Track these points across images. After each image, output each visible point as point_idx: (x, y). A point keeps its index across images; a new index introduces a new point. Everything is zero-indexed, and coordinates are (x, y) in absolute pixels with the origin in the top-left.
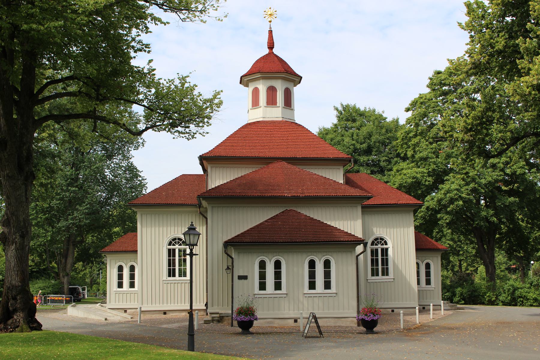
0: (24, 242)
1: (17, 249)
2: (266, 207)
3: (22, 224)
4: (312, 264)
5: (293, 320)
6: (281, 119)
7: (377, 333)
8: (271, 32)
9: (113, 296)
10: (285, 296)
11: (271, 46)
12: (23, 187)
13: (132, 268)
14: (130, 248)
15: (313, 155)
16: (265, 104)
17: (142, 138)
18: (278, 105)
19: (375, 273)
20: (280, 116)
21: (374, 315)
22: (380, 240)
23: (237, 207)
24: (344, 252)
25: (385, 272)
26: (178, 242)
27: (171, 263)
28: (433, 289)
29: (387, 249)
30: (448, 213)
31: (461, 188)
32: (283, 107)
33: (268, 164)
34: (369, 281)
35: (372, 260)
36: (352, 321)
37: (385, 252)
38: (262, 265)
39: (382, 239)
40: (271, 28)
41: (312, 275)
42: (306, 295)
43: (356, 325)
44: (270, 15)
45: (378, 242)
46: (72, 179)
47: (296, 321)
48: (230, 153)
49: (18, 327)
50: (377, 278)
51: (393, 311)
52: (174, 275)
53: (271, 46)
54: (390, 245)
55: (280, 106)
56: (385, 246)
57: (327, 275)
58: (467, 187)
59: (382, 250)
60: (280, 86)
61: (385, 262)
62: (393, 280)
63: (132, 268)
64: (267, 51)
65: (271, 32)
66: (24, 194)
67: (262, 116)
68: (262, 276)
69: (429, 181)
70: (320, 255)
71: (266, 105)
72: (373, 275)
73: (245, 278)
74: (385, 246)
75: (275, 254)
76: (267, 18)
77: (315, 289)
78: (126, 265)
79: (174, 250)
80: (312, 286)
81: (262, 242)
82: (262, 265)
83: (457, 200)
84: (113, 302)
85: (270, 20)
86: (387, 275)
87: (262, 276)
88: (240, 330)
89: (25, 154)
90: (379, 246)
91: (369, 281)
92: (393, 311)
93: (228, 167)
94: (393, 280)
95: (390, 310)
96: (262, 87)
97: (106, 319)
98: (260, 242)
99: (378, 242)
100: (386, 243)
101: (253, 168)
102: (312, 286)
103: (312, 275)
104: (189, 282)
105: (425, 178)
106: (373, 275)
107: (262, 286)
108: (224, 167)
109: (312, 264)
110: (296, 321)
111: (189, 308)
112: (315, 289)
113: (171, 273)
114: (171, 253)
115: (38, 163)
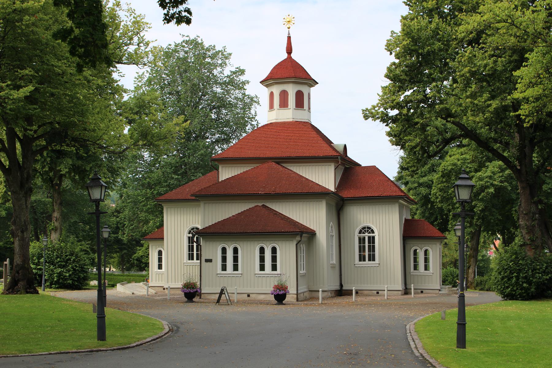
0: (24, 235)
1: (19, 240)
2: (240, 203)
3: (23, 223)
4: (262, 250)
5: (246, 295)
6: (291, 120)
7: (285, 304)
8: (289, 38)
9: (154, 276)
10: (241, 275)
11: (289, 50)
12: (24, 198)
13: (160, 253)
14: (160, 237)
15: (307, 154)
16: (278, 107)
17: (256, 120)
18: (289, 107)
19: (362, 258)
20: (291, 117)
21: (280, 291)
22: (369, 230)
23: (227, 203)
24: (211, 241)
25: (372, 258)
26: (368, 231)
27: (191, 249)
28: (432, 274)
29: (374, 238)
30: (482, 200)
31: (494, 174)
32: (295, 109)
33: (264, 162)
34: (356, 265)
35: (360, 247)
36: (293, 297)
37: (372, 240)
38: (224, 250)
39: (370, 228)
40: (289, 34)
41: (262, 259)
42: (256, 275)
43: (296, 300)
44: (289, 22)
45: (365, 231)
46: (176, 167)
47: (249, 296)
48: (237, 155)
49: (19, 291)
50: (191, 261)
51: (378, 293)
52: (364, 260)
53: (289, 50)
54: (376, 234)
55: (291, 107)
56: (371, 235)
57: (274, 259)
58: (501, 174)
59: (369, 237)
60: (292, 90)
61: (372, 248)
62: (378, 265)
63: (160, 253)
64: (285, 56)
65: (289, 38)
66: (24, 203)
67: (275, 118)
68: (224, 259)
69: (470, 168)
70: (268, 243)
71: (279, 108)
72: (360, 260)
73: (209, 261)
74: (371, 235)
75: (272, 242)
76: (286, 24)
77: (264, 270)
78: (421, 249)
79: (364, 238)
80: (262, 268)
81: (221, 233)
82: (224, 250)
83: (487, 187)
84: (154, 282)
85: (288, 26)
86: (374, 260)
87: (224, 259)
88: (186, 299)
89: (26, 176)
90: (367, 234)
91: (356, 265)
92: (378, 293)
93: (236, 167)
94: (378, 265)
95: (376, 292)
96: (277, 90)
97: (133, 294)
98: (219, 233)
99: (365, 231)
100: (373, 232)
101: (248, 166)
102: (262, 268)
103: (262, 259)
104: (199, 264)
105: (467, 164)
106: (360, 260)
107: (224, 268)
108: (232, 167)
109: (262, 250)
110: (249, 296)
111: (295, 292)
112: (264, 270)
113: (191, 257)
114: (191, 240)
115: (101, 164)
